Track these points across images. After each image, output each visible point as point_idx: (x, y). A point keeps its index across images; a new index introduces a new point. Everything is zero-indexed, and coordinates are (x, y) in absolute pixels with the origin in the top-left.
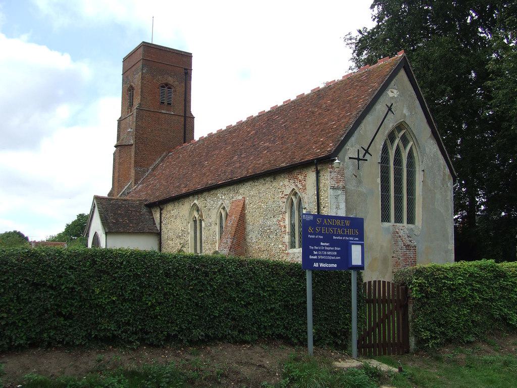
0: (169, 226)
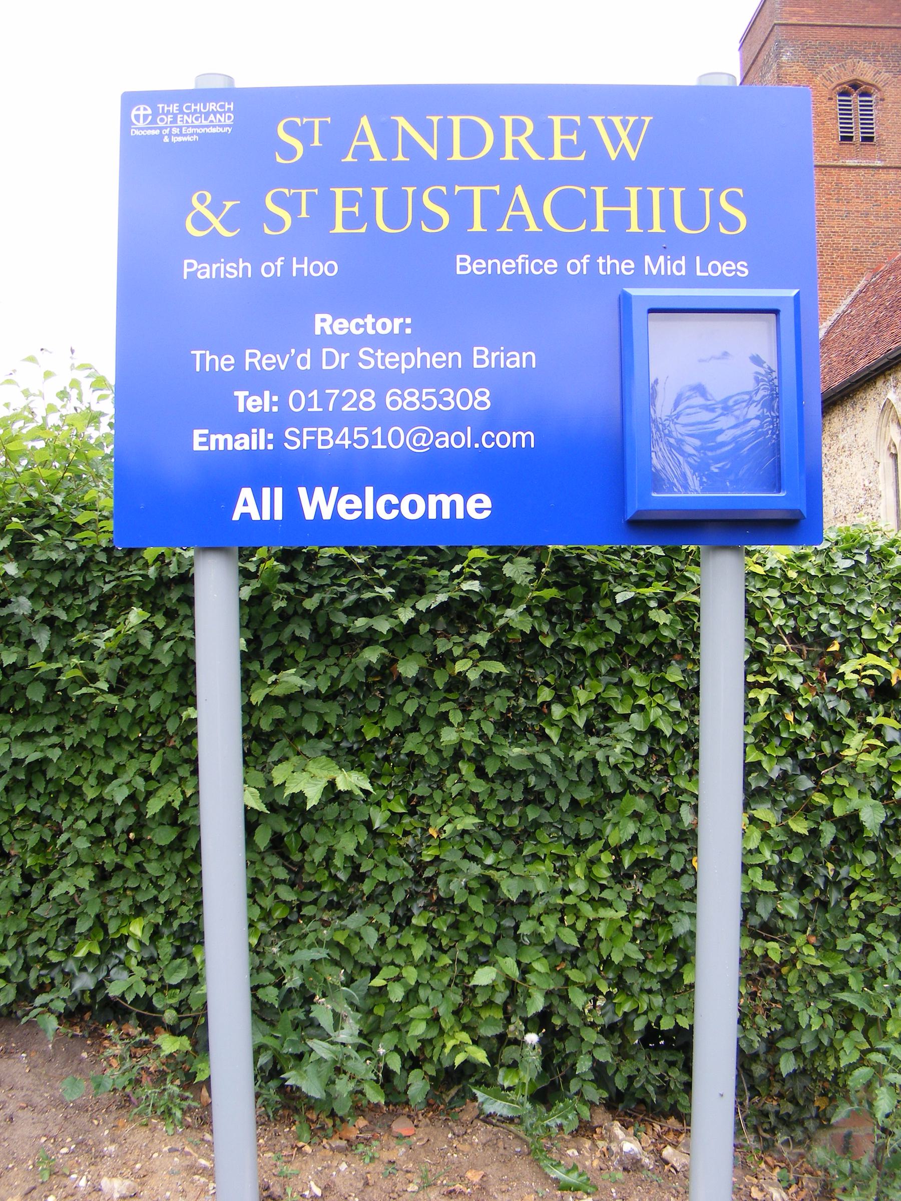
0: (838, 480)
